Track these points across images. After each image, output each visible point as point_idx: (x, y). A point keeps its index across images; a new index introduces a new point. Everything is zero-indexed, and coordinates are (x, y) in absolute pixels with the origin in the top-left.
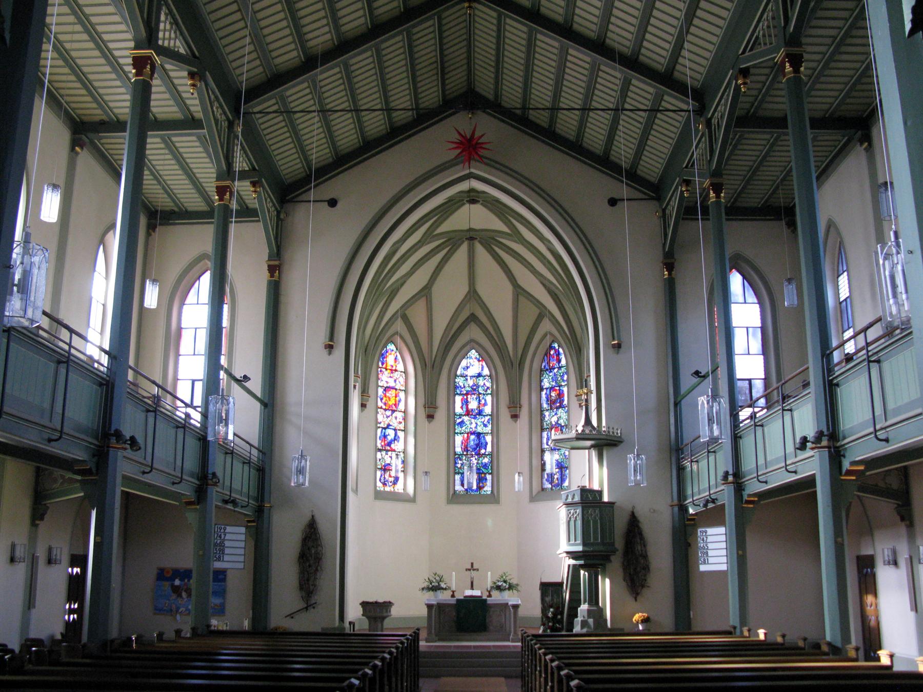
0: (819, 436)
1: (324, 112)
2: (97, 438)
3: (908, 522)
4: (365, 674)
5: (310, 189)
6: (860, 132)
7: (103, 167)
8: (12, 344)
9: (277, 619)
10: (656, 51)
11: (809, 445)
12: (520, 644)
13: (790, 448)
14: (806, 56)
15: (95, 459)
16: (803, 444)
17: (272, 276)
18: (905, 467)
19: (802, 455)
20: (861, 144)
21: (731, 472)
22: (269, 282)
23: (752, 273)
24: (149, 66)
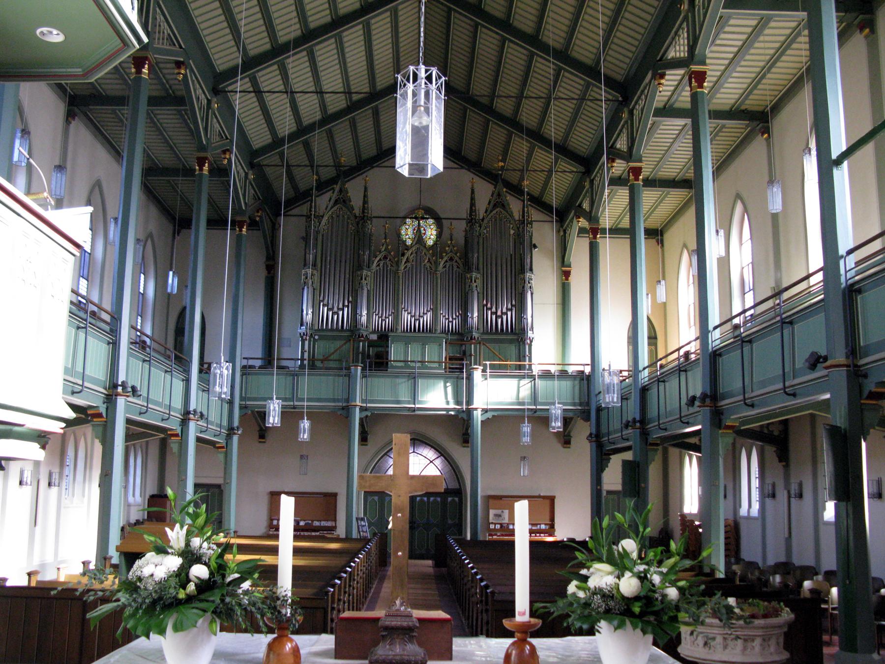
0: (704, 396)
1: (291, 93)
2: (105, 389)
3: (784, 463)
4: (336, 584)
5: (237, 81)
6: (761, 125)
7: (108, 151)
8: (88, 337)
9: (481, 537)
10: (585, 47)
11: (697, 403)
12: (469, 538)
13: (684, 401)
14: (708, 73)
15: (105, 406)
16: (692, 401)
17: (269, 273)
18: (787, 420)
19: (692, 410)
20: (762, 135)
21: (638, 418)
22: (267, 278)
23: (479, 524)
24: (146, 66)
